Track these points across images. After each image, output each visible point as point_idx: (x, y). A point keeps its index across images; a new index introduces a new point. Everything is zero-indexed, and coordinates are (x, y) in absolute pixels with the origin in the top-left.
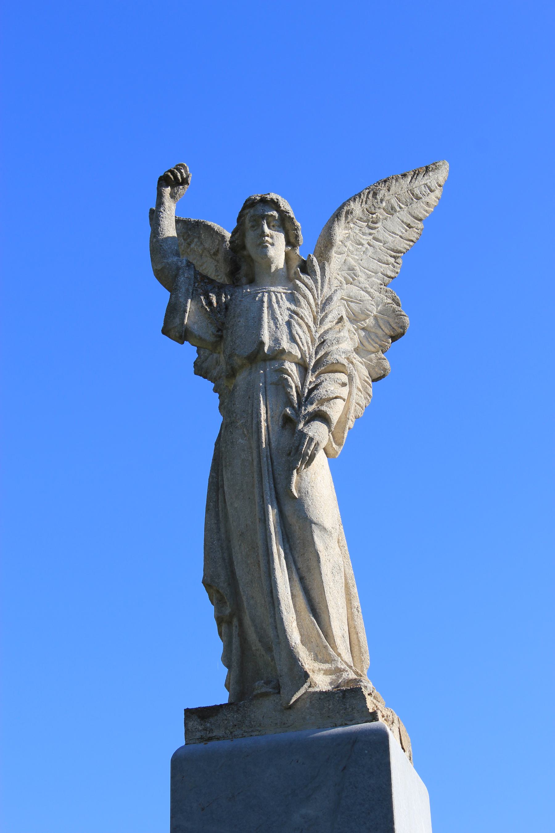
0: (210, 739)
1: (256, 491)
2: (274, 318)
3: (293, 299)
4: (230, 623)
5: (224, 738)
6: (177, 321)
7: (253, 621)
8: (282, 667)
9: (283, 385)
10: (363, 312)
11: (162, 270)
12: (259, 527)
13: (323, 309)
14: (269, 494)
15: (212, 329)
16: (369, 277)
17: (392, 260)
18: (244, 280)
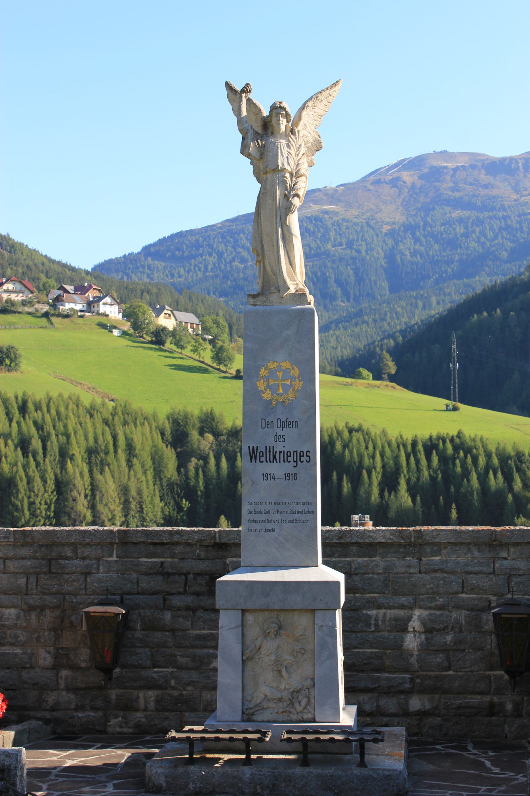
0: (256, 305)
1: (274, 221)
2: (282, 155)
3: (288, 147)
4: (260, 262)
5: (261, 305)
6: (247, 151)
7: (269, 264)
8: (281, 284)
9: (285, 182)
10: (308, 141)
11: (242, 129)
12: (275, 234)
13: (298, 150)
14: (279, 224)
15: (259, 154)
16: (311, 126)
17: (319, 119)
18: (270, 134)
